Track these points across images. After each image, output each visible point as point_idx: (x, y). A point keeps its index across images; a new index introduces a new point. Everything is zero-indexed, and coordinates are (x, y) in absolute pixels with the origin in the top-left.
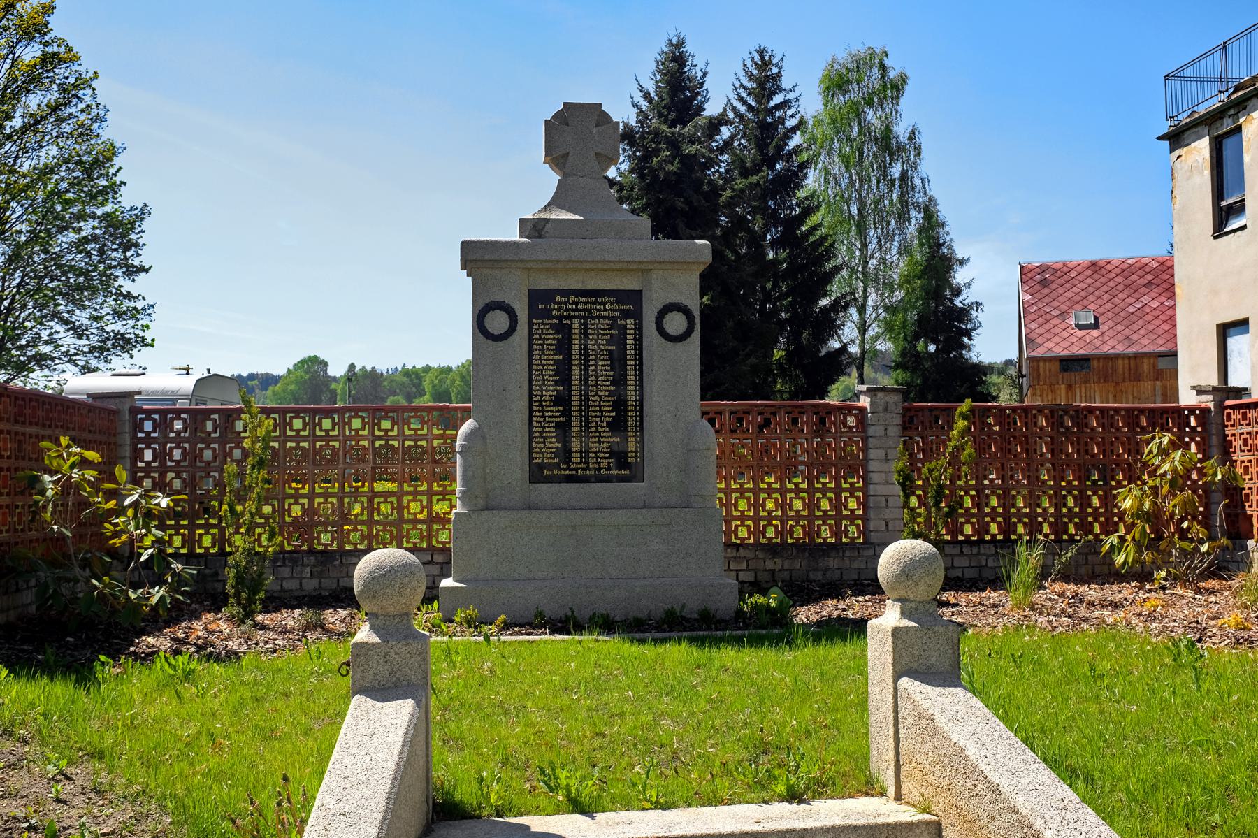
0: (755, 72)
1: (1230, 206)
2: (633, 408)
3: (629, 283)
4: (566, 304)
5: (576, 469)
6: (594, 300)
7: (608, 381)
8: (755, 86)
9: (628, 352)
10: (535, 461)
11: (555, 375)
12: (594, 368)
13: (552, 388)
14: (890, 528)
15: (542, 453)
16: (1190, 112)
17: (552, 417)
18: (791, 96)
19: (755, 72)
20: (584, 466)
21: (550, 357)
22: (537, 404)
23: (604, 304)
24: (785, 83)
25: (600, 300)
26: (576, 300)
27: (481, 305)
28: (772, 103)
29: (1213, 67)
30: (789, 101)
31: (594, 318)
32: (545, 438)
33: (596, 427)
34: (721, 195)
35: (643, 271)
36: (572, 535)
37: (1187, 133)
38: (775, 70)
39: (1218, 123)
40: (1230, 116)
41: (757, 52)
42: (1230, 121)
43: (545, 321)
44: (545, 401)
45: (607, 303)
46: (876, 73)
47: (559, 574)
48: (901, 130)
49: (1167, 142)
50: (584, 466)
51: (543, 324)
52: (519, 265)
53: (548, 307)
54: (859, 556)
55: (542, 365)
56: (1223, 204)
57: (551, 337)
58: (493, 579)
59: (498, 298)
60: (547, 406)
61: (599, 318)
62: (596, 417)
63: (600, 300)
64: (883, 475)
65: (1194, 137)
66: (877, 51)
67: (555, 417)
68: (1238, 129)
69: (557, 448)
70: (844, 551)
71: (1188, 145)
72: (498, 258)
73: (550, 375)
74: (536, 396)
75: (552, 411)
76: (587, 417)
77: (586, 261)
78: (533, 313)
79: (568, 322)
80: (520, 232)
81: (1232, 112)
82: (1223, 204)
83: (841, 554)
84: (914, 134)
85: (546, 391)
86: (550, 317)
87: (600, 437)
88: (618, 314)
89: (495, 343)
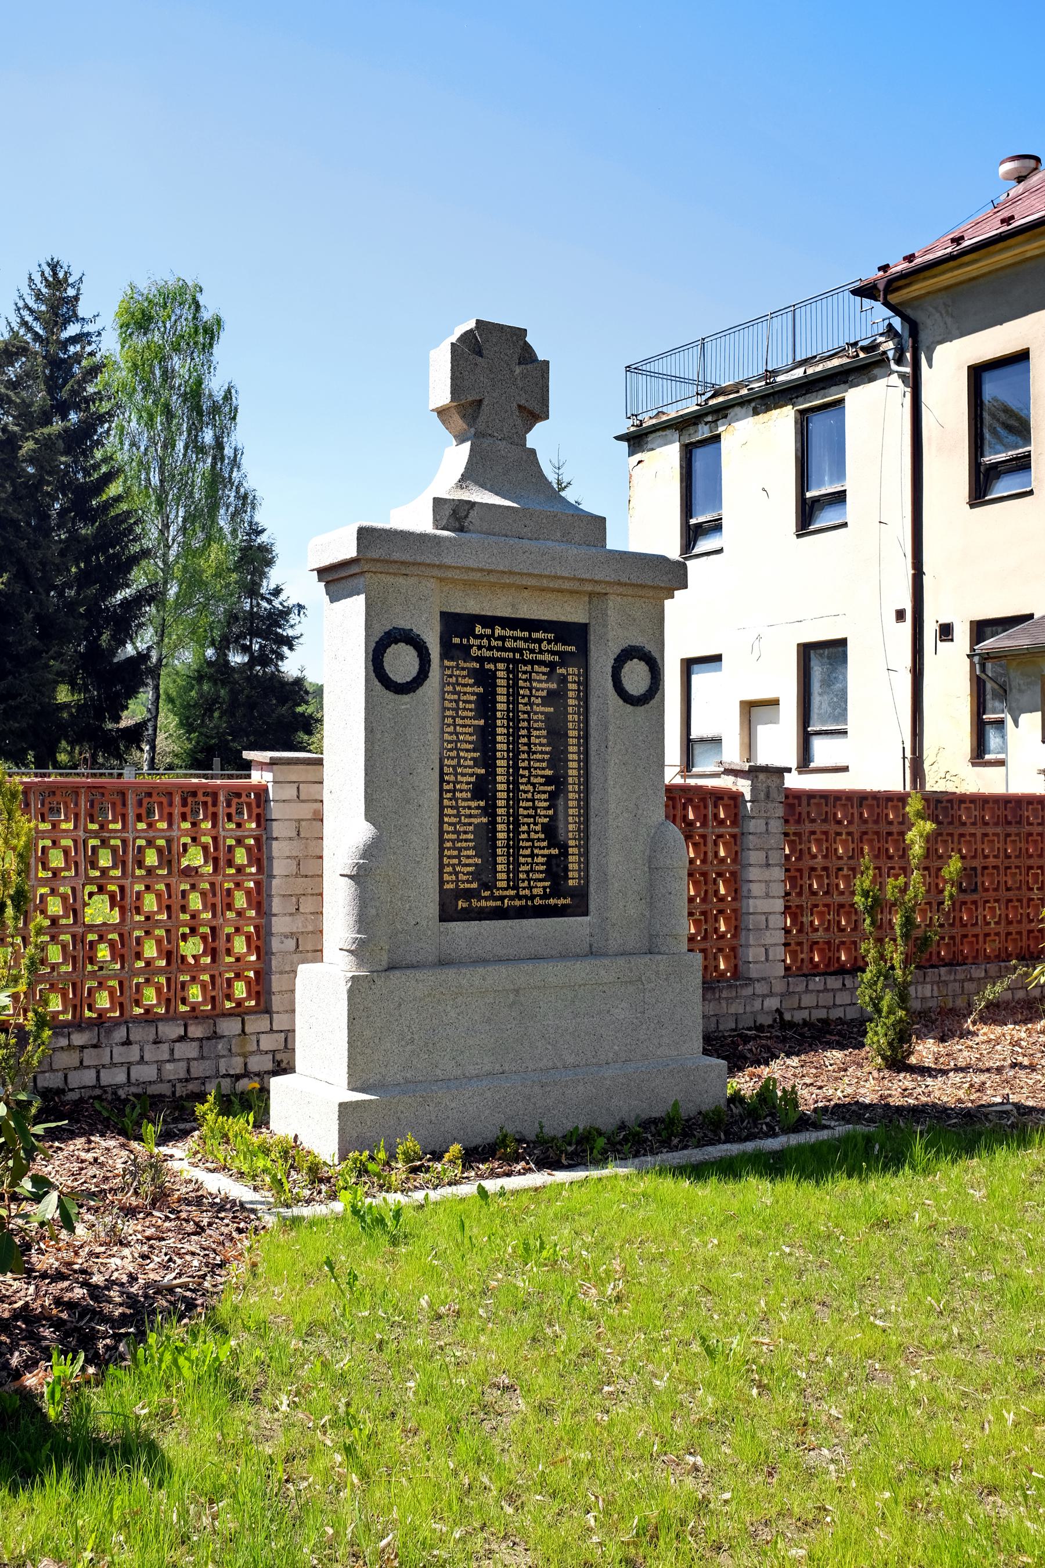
0: (44, 290)
1: (699, 526)
2: (575, 803)
3: (572, 613)
4: (489, 637)
5: (502, 898)
6: (527, 634)
7: (543, 761)
8: (43, 308)
9: (570, 717)
10: (446, 886)
11: (474, 750)
12: (525, 740)
13: (470, 771)
14: (771, 958)
15: (457, 874)
16: (655, 412)
17: (470, 816)
18: (89, 328)
19: (44, 290)
20: (513, 893)
21: (468, 722)
22: (449, 795)
23: (539, 641)
24: (82, 311)
25: (535, 635)
26: (503, 633)
27: (378, 634)
28: (65, 335)
29: (687, 365)
30: (88, 334)
31: (526, 663)
32: (460, 849)
33: (528, 833)
34: (20, 447)
35: (591, 595)
36: (514, 1003)
37: (651, 437)
38: (71, 292)
39: (692, 429)
40: (706, 423)
41: (49, 265)
42: (706, 428)
43: (462, 664)
44: (461, 791)
45: (542, 640)
46: (187, 313)
47: (497, 1067)
48: (215, 385)
49: (626, 444)
50: (513, 893)
51: (457, 667)
52: (436, 572)
53: (465, 641)
54: (737, 997)
55: (457, 734)
56: (693, 521)
57: (469, 689)
58: (407, 1081)
59: (403, 624)
60: (464, 800)
61: (533, 663)
62: (528, 816)
63: (535, 635)
64: (763, 885)
65: (659, 441)
66: (190, 284)
67: (475, 816)
68: (717, 438)
69: (476, 865)
70: (721, 991)
71: (653, 449)
72: (411, 560)
73: (467, 751)
74: (448, 782)
75: (470, 808)
76: (516, 816)
77: (529, 575)
78: (448, 650)
79: (491, 666)
80: (435, 520)
81: (709, 418)
82: (693, 521)
83: (717, 996)
84: (230, 393)
85: (463, 775)
86: (468, 657)
87: (533, 847)
88: (557, 658)
89: (397, 696)
